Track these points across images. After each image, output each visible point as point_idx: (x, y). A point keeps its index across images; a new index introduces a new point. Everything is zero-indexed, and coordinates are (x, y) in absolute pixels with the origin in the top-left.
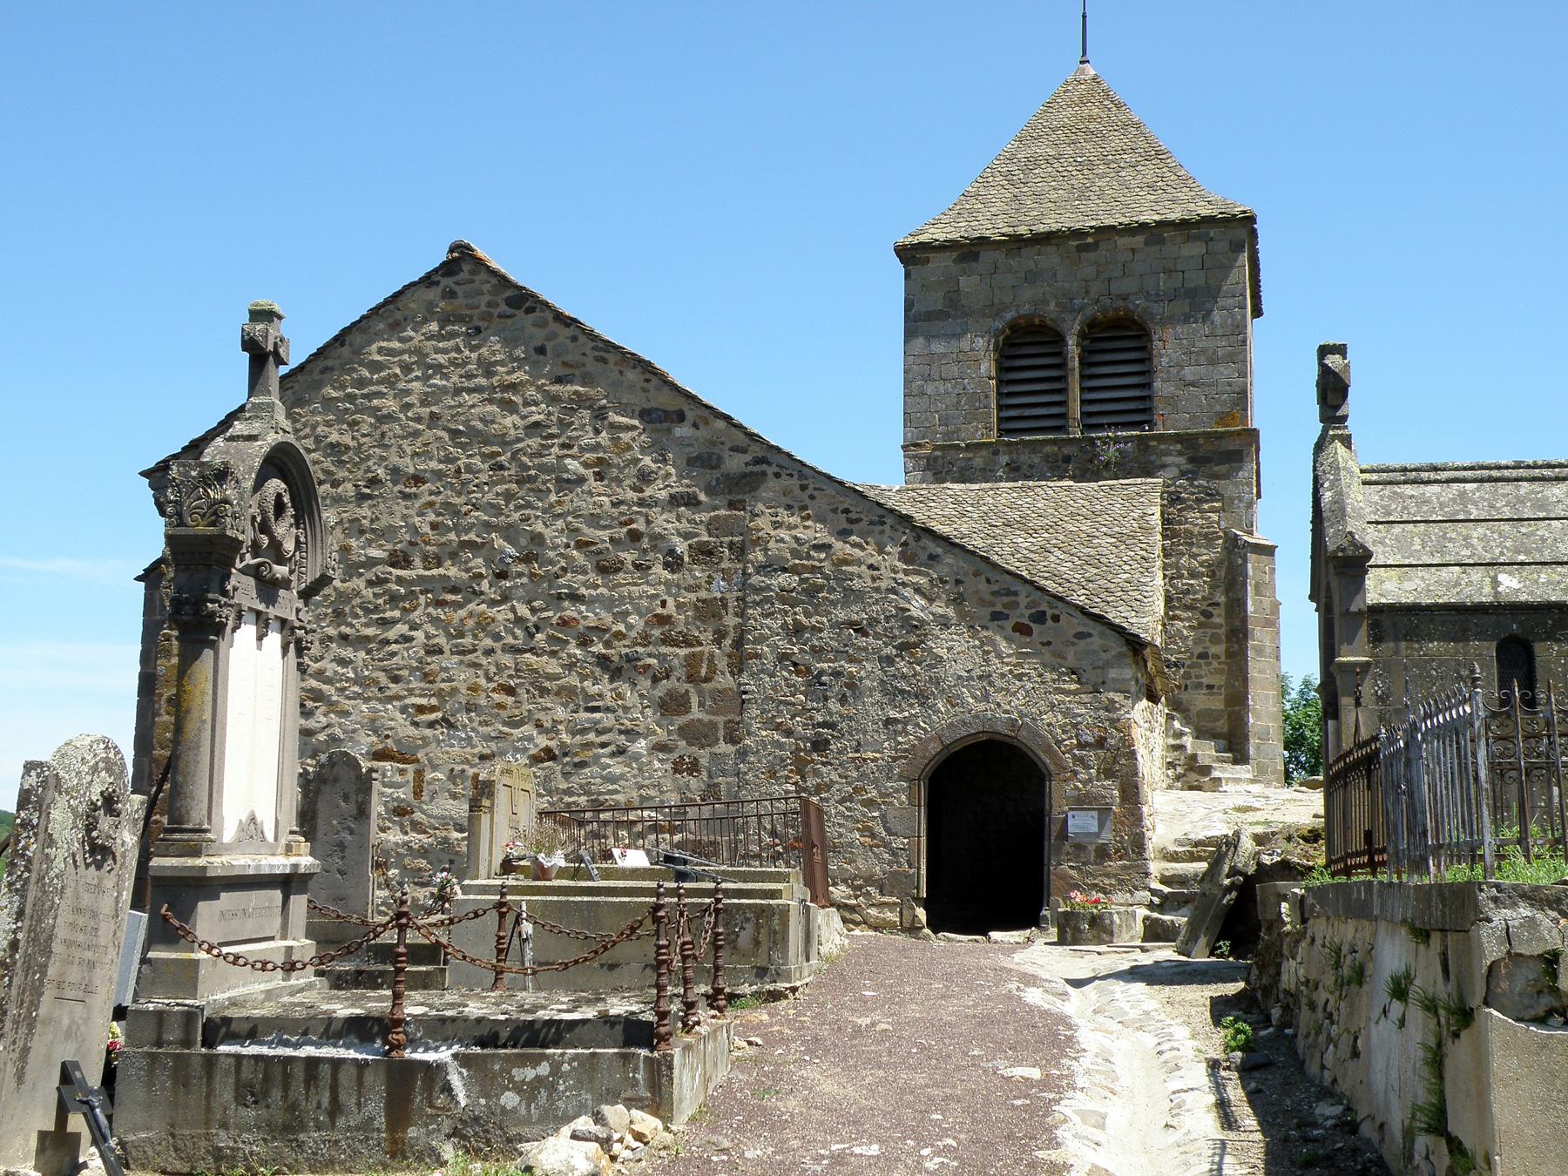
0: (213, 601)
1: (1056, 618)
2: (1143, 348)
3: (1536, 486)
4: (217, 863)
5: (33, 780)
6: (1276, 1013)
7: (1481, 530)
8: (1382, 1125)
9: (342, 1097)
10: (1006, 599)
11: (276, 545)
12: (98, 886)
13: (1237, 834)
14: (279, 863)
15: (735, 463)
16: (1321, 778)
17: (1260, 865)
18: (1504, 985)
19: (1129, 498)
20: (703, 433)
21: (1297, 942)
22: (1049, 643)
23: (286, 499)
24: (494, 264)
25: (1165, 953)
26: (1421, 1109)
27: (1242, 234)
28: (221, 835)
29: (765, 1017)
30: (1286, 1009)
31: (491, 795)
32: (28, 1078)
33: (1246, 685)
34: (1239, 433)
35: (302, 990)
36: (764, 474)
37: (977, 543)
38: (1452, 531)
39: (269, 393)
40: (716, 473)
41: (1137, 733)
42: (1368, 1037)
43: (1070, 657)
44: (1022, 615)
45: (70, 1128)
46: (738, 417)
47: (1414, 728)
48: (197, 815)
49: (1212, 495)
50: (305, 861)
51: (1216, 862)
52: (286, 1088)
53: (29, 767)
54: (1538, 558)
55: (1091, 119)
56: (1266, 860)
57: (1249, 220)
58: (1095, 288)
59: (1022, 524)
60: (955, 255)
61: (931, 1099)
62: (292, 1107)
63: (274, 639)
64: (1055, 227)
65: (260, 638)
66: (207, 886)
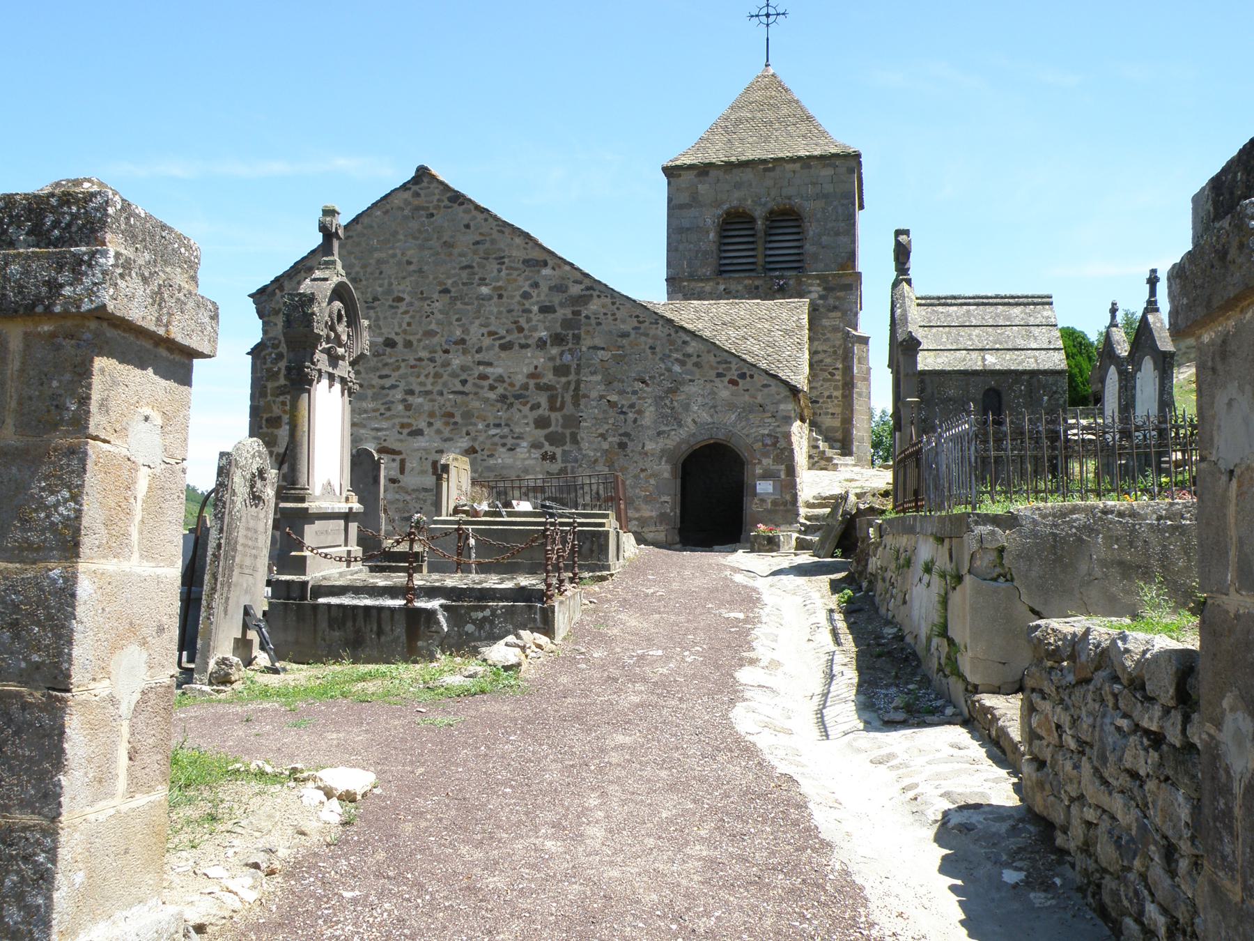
0: (308, 368)
1: (752, 376)
2: (799, 226)
3: (1006, 308)
4: (313, 506)
5: (224, 461)
6: (865, 584)
7: (977, 331)
8: (916, 636)
9: (383, 626)
10: (724, 366)
11: (338, 336)
12: (257, 517)
13: (847, 492)
14: (343, 507)
15: (575, 290)
16: (891, 463)
17: (858, 509)
18: (978, 563)
19: (791, 310)
20: (557, 273)
21: (877, 548)
22: (748, 390)
23: (343, 312)
24: (441, 178)
25: (806, 558)
26: (935, 625)
27: (854, 164)
28: (313, 490)
29: (597, 589)
30: (870, 582)
31: (447, 472)
32: (229, 612)
33: (852, 413)
34: (851, 274)
35: (357, 573)
36: (591, 296)
37: (707, 334)
38: (963, 331)
39: (333, 255)
40: (565, 295)
41: (794, 439)
42: (911, 594)
43: (759, 397)
44: (733, 374)
45: (249, 637)
46: (577, 264)
47: (941, 436)
48: (303, 480)
49: (835, 308)
50: (356, 506)
51: (835, 508)
52: (354, 620)
53: (222, 455)
54: (1006, 347)
55: (771, 97)
56: (862, 507)
57: (857, 156)
58: (773, 193)
59: (732, 324)
60: (695, 172)
61: (687, 629)
62: (357, 631)
63: (337, 387)
64: (751, 157)
65: (331, 386)
66: (307, 517)
